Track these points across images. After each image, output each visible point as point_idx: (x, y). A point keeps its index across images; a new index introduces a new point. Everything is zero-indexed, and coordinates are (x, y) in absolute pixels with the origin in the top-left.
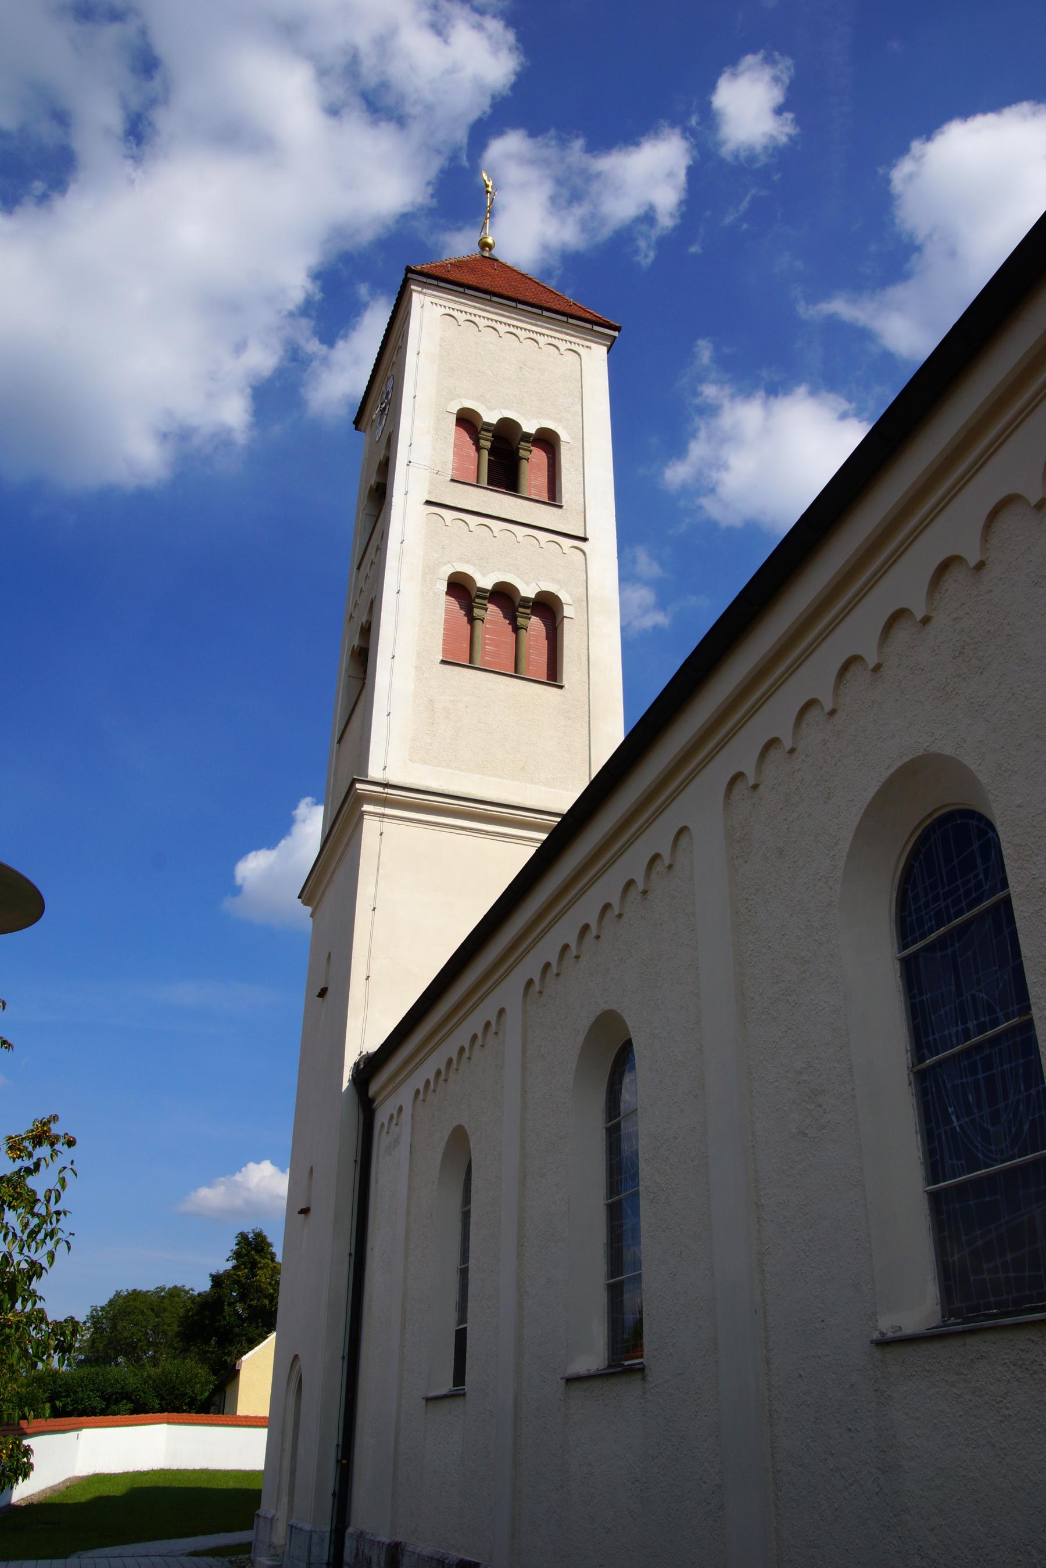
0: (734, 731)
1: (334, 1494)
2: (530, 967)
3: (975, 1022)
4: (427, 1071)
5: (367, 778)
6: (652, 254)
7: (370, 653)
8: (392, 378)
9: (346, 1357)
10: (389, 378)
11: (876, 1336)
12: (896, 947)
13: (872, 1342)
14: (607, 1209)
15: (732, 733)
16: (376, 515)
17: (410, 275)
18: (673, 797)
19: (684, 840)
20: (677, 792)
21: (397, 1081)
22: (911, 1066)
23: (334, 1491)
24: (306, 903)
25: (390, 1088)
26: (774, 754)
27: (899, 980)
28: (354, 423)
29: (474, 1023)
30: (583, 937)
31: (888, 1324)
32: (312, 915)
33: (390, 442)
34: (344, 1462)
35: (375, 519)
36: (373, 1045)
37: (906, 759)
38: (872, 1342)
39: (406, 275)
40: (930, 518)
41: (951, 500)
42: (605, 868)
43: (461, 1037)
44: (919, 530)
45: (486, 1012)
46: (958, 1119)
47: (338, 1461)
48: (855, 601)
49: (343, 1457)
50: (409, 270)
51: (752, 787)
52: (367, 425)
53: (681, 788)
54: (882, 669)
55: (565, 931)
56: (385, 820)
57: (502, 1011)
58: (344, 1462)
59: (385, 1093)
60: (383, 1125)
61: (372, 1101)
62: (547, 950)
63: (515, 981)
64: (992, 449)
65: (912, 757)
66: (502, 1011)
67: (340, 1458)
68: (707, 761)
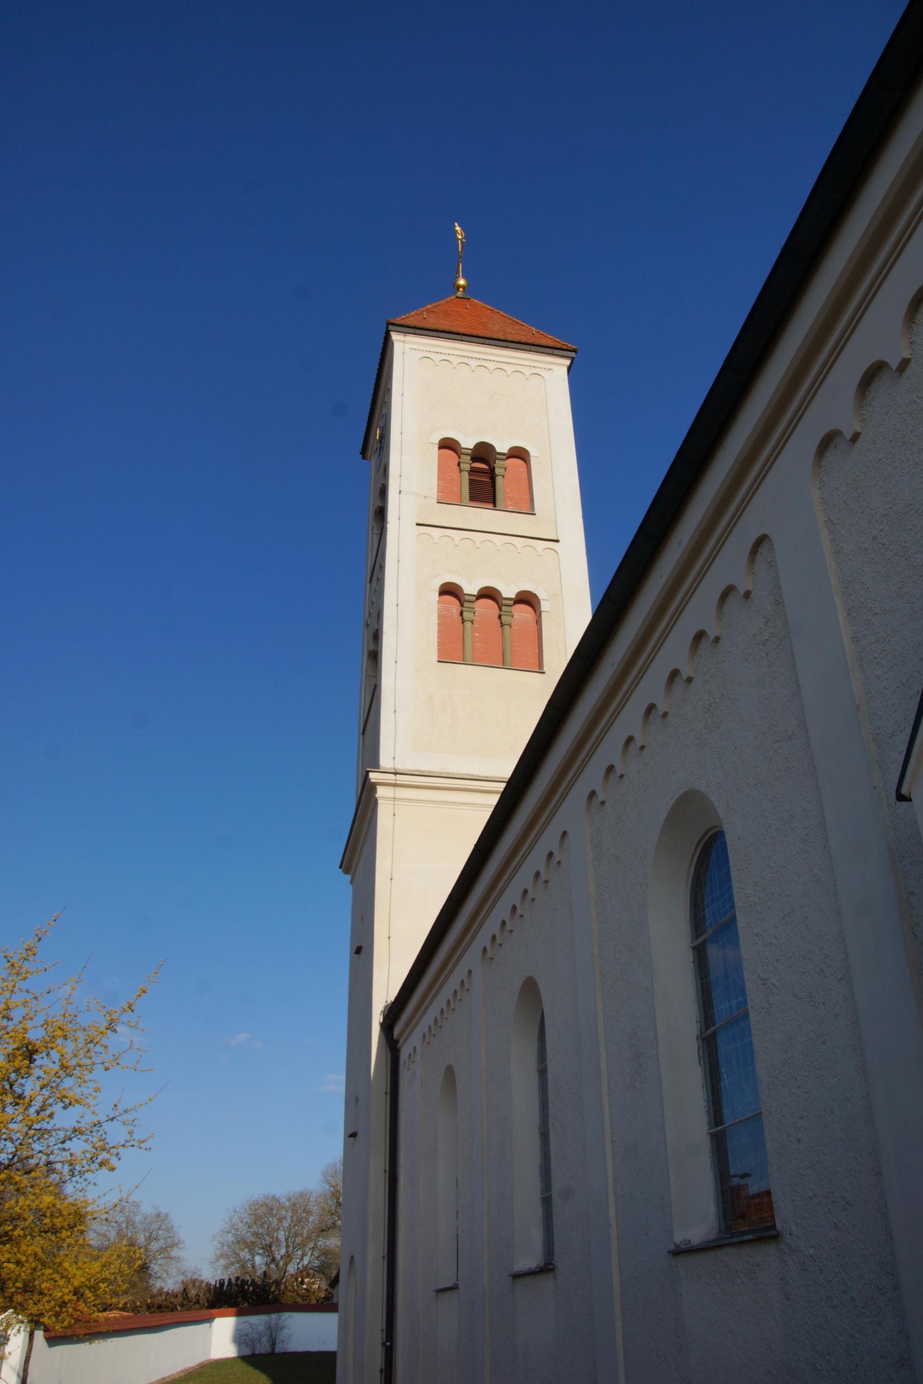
0: (596, 744)
1: (381, 1371)
2: (482, 939)
3: (736, 1001)
4: (428, 1020)
5: (379, 769)
6: (340, 1242)
7: (386, 509)
8: (385, 416)
9: (386, 1257)
10: (383, 415)
11: (672, 1247)
12: (690, 938)
13: (669, 1252)
14: (712, 1141)
15: (630, 691)
16: (379, 533)
17: (390, 328)
18: (563, 797)
19: (764, 549)
20: (577, 775)
21: (412, 1025)
22: (699, 1034)
23: (381, 1368)
24: (346, 872)
25: (407, 1032)
26: (731, 601)
27: (692, 965)
28: (361, 453)
29: (453, 983)
30: (723, 604)
31: (679, 1237)
32: (351, 882)
33: (384, 470)
34: (388, 1344)
35: (378, 538)
36: (392, 994)
37: (681, 792)
38: (669, 1252)
39: (387, 327)
40: (660, 643)
41: (741, 515)
42: (547, 822)
43: (446, 993)
44: (657, 647)
45: (459, 973)
46: (728, 1078)
47: (383, 1344)
48: (753, 490)
49: (387, 1340)
50: (389, 324)
51: (744, 596)
52: (371, 455)
53: (577, 775)
54: (668, 716)
55: (501, 911)
56: (394, 782)
57: (470, 972)
58: (388, 1344)
59: (405, 1036)
60: (405, 1061)
61: (397, 1042)
62: (491, 926)
63: (474, 953)
64: (711, 559)
65: (684, 791)
66: (470, 972)
67: (384, 1341)
68: (608, 726)
